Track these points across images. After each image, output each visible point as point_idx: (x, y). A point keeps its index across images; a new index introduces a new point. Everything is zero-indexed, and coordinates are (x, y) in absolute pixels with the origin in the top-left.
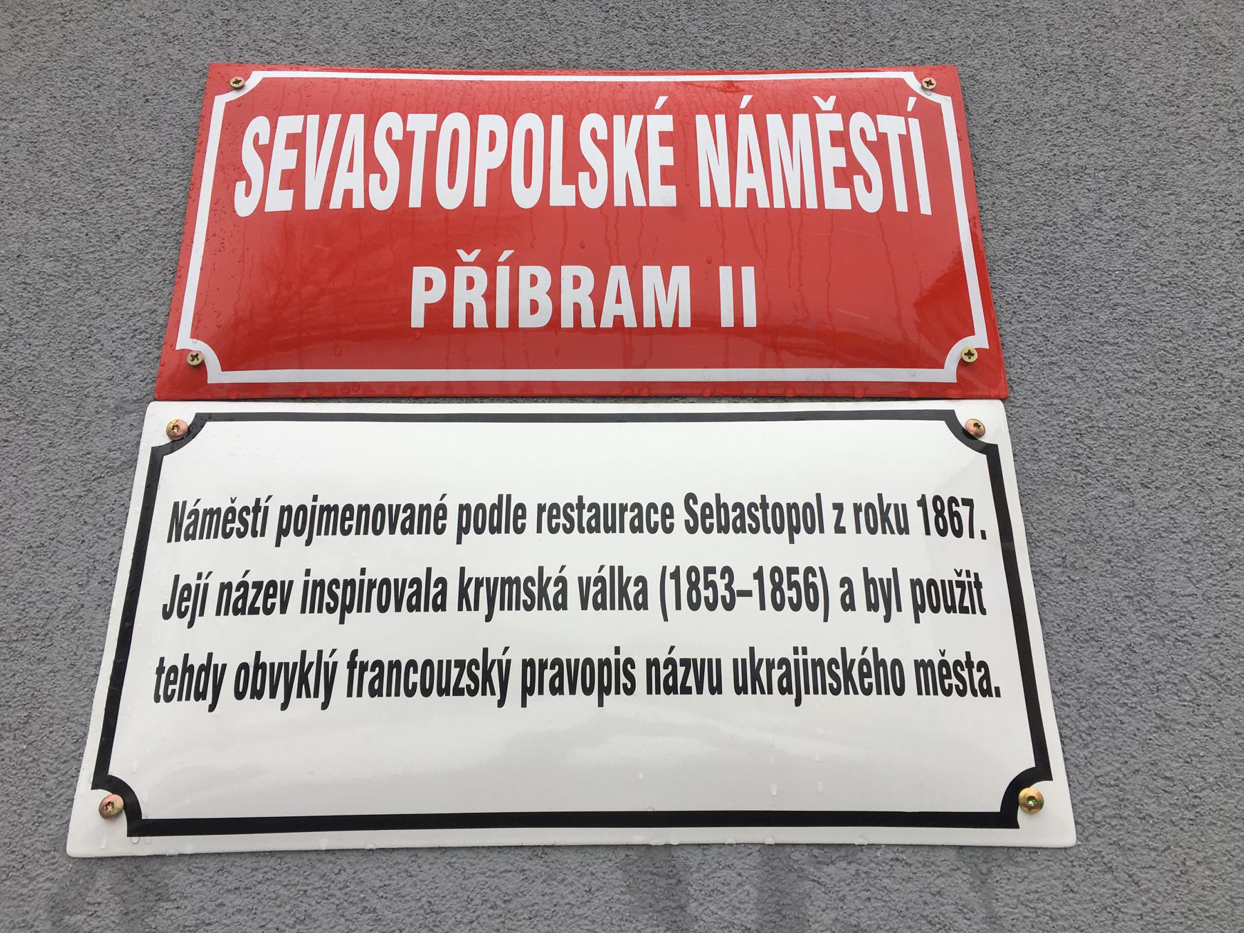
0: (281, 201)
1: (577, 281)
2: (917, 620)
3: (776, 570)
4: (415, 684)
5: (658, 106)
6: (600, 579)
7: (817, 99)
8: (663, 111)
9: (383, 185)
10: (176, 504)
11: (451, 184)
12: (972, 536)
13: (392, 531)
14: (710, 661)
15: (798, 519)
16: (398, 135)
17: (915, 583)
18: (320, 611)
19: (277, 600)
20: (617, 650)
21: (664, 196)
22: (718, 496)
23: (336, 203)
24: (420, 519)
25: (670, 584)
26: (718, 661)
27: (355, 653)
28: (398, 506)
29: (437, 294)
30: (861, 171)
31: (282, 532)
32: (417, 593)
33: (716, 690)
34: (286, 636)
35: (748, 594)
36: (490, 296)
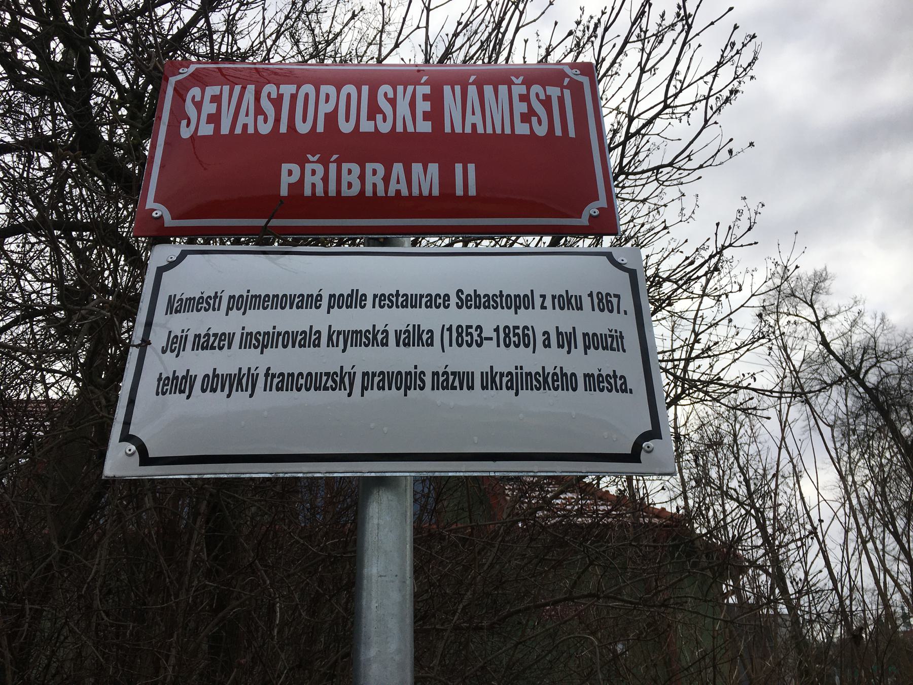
0: (206, 130)
1: (375, 171)
2: (586, 353)
3: (506, 327)
4: (302, 385)
5: (422, 81)
6: (407, 331)
7: (513, 78)
8: (425, 84)
9: (266, 121)
10: (170, 296)
11: (304, 121)
12: (619, 312)
13: (291, 308)
14: (468, 373)
15: (521, 302)
16: (274, 95)
17: (585, 335)
18: (250, 348)
19: (226, 343)
20: (416, 367)
21: (425, 127)
22: (475, 291)
23: (238, 130)
24: (310, 301)
25: (446, 334)
26: (473, 373)
27: (269, 369)
28: (401, 331)
29: (295, 178)
30: (536, 115)
31: (229, 309)
32: (305, 338)
33: (470, 388)
34: (228, 361)
35: (491, 339)
36: (325, 179)
